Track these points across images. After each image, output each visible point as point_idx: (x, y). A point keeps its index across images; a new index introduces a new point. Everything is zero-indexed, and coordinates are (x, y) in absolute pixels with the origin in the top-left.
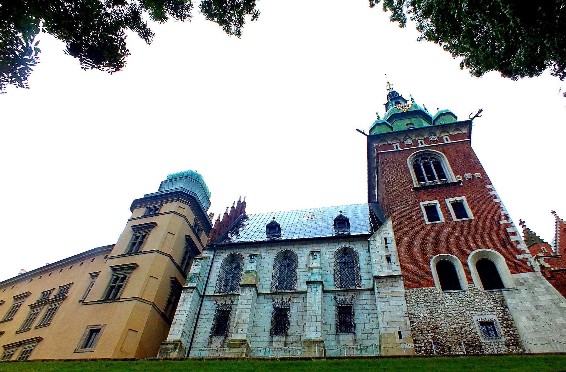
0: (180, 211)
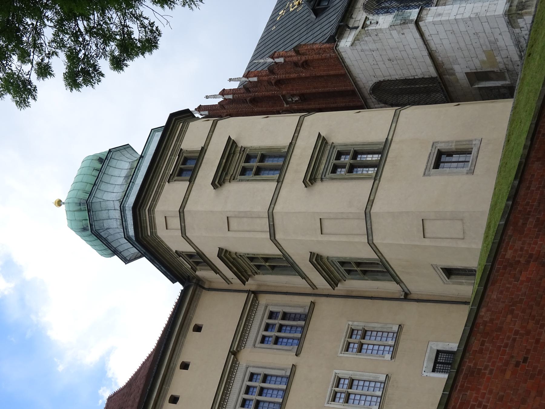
0: (175, 223)
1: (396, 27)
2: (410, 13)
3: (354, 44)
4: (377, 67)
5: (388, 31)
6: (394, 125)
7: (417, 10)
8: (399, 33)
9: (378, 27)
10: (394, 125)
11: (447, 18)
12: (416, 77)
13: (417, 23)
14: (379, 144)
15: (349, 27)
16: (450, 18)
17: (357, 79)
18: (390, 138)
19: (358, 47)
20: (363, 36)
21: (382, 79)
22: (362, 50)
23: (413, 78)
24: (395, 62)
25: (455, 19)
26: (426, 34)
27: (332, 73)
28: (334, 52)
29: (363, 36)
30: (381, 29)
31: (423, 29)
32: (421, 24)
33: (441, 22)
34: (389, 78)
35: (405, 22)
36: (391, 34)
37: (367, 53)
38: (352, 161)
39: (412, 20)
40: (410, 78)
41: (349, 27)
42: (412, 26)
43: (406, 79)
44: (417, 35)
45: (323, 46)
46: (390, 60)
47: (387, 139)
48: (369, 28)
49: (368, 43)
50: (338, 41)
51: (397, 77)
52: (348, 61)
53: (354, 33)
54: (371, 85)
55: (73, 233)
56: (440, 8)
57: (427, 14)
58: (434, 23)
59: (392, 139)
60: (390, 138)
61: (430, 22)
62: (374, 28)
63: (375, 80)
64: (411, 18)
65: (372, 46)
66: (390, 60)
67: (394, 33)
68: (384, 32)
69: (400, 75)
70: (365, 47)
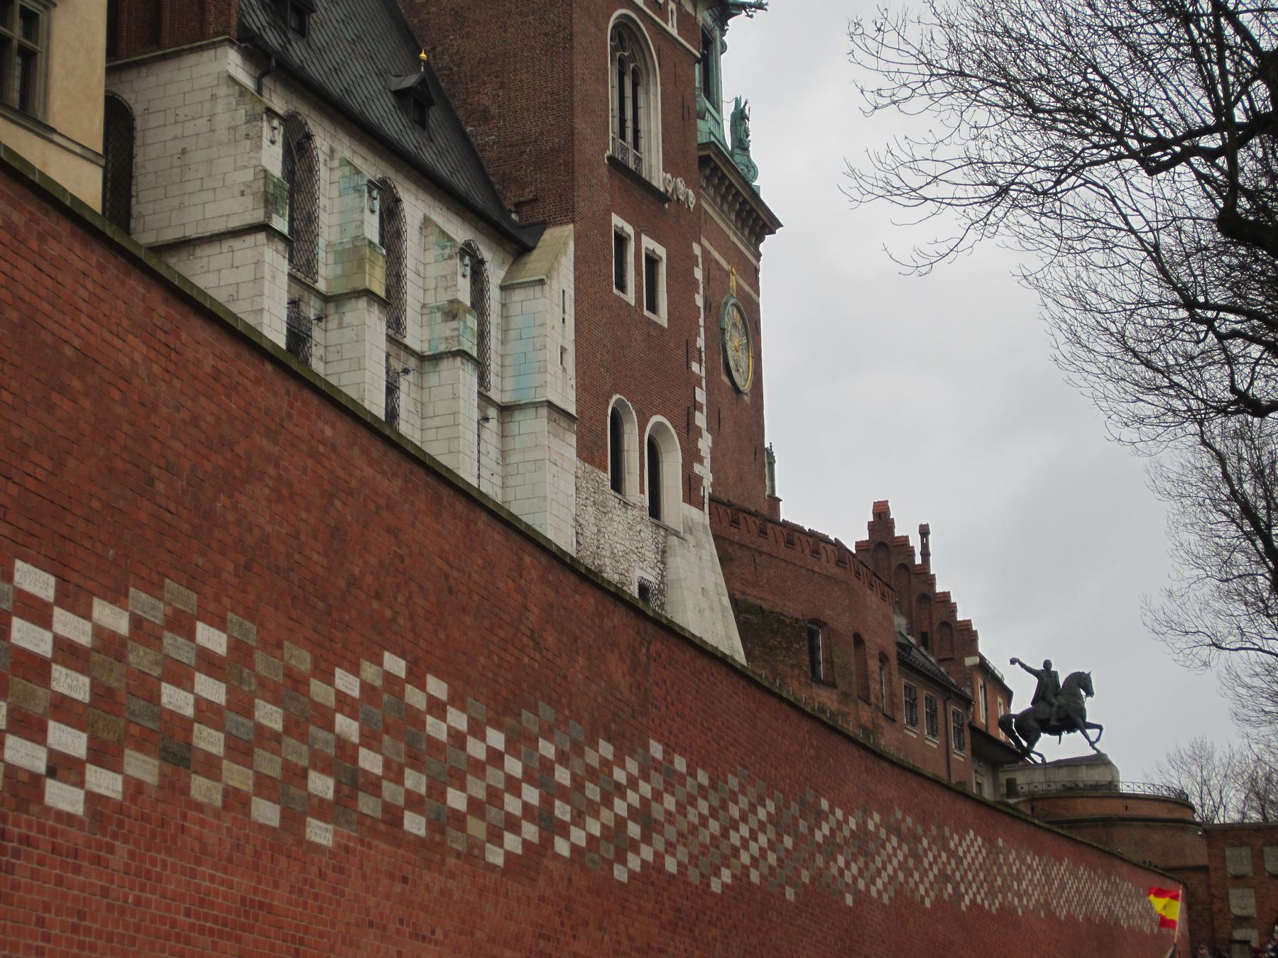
1: (261, 183)
2: (283, 216)
3: (231, 83)
4: (171, 119)
5: (253, 162)
6: (78, 149)
7: (286, 231)
8: (247, 185)
9: (266, 142)
10: (78, 149)
11: (266, 292)
12: (134, 201)
13: (264, 228)
14: (45, 113)
15: (262, 75)
16: (266, 299)
17: (144, 71)
18: (56, 138)
19: (223, 91)
20: (248, 107)
21: (138, 124)
22: (214, 97)
23: (134, 193)
24: (176, 162)
25: (261, 310)
26: (237, 243)
27: (167, 16)
28: (217, 34)
29: (248, 107)
30: (260, 147)
31: (249, 240)
32: (261, 237)
33: (258, 279)
34: (138, 141)
35: (270, 202)
36: (245, 167)
37: (207, 106)
38: (15, 43)
39: (270, 218)
40: (134, 188)
41: (262, 75)
42: (258, 216)
43: (131, 177)
44: (235, 223)
45: (233, 11)
46: (184, 151)
47: (54, 130)
48: (265, 124)
49: (229, 113)
50: (240, 47)
51: (138, 159)
52: (193, 59)
53: (249, 83)
54: (125, 96)
55: (1114, 762)
56: (286, 279)
57: (277, 251)
58: (258, 263)
59: (51, 141)
60: (56, 138)
61: (262, 255)
62: (265, 134)
63: (137, 110)
64: (274, 216)
65: (223, 120)
66: (184, 151)
67: (248, 175)
68: (252, 154)
69: (144, 167)
70: (220, 106)
